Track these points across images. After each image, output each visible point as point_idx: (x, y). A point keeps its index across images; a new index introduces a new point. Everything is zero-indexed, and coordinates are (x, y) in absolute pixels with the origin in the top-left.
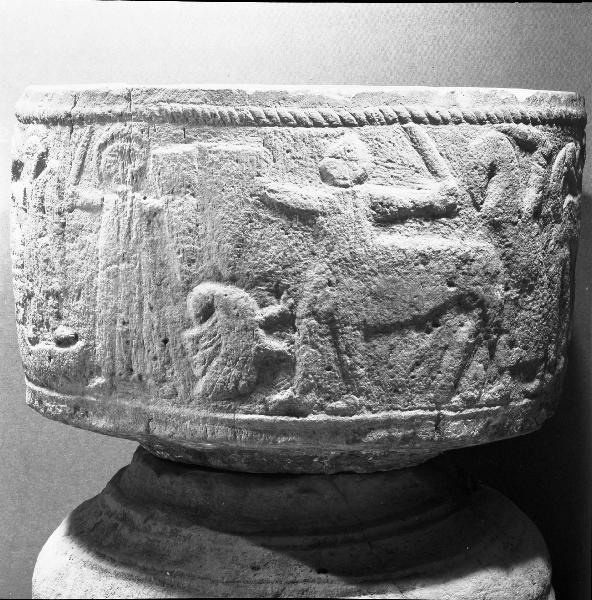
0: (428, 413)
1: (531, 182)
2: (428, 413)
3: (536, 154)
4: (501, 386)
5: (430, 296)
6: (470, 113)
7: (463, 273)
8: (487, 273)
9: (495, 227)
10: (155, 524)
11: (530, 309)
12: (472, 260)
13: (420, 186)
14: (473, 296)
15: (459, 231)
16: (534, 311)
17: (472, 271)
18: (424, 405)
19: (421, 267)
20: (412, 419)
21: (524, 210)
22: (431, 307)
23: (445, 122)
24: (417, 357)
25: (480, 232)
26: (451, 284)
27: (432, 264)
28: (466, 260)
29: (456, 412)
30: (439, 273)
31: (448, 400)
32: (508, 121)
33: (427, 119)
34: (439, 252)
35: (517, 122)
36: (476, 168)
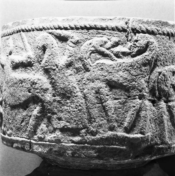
0: (26, 140)
1: (65, 53)
2: (26, 140)
3: (68, 42)
4: (55, 135)
5: (23, 96)
6: (37, 27)
7: (33, 88)
8: (42, 89)
9: (47, 71)
11: (69, 106)
13: (22, 55)
14: (37, 97)
15: (33, 72)
16: (72, 107)
17: (36, 87)
18: (25, 137)
19: (21, 85)
20: (22, 141)
21: (60, 65)
22: (24, 100)
23: (30, 31)
24: (22, 118)
25: (41, 72)
26: (30, 92)
27: (23, 84)
28: (34, 83)
29: (36, 141)
30: (25, 87)
31: (33, 137)
32: (52, 29)
33: (25, 30)
34: (25, 79)
35: (56, 29)
36: (37, 47)
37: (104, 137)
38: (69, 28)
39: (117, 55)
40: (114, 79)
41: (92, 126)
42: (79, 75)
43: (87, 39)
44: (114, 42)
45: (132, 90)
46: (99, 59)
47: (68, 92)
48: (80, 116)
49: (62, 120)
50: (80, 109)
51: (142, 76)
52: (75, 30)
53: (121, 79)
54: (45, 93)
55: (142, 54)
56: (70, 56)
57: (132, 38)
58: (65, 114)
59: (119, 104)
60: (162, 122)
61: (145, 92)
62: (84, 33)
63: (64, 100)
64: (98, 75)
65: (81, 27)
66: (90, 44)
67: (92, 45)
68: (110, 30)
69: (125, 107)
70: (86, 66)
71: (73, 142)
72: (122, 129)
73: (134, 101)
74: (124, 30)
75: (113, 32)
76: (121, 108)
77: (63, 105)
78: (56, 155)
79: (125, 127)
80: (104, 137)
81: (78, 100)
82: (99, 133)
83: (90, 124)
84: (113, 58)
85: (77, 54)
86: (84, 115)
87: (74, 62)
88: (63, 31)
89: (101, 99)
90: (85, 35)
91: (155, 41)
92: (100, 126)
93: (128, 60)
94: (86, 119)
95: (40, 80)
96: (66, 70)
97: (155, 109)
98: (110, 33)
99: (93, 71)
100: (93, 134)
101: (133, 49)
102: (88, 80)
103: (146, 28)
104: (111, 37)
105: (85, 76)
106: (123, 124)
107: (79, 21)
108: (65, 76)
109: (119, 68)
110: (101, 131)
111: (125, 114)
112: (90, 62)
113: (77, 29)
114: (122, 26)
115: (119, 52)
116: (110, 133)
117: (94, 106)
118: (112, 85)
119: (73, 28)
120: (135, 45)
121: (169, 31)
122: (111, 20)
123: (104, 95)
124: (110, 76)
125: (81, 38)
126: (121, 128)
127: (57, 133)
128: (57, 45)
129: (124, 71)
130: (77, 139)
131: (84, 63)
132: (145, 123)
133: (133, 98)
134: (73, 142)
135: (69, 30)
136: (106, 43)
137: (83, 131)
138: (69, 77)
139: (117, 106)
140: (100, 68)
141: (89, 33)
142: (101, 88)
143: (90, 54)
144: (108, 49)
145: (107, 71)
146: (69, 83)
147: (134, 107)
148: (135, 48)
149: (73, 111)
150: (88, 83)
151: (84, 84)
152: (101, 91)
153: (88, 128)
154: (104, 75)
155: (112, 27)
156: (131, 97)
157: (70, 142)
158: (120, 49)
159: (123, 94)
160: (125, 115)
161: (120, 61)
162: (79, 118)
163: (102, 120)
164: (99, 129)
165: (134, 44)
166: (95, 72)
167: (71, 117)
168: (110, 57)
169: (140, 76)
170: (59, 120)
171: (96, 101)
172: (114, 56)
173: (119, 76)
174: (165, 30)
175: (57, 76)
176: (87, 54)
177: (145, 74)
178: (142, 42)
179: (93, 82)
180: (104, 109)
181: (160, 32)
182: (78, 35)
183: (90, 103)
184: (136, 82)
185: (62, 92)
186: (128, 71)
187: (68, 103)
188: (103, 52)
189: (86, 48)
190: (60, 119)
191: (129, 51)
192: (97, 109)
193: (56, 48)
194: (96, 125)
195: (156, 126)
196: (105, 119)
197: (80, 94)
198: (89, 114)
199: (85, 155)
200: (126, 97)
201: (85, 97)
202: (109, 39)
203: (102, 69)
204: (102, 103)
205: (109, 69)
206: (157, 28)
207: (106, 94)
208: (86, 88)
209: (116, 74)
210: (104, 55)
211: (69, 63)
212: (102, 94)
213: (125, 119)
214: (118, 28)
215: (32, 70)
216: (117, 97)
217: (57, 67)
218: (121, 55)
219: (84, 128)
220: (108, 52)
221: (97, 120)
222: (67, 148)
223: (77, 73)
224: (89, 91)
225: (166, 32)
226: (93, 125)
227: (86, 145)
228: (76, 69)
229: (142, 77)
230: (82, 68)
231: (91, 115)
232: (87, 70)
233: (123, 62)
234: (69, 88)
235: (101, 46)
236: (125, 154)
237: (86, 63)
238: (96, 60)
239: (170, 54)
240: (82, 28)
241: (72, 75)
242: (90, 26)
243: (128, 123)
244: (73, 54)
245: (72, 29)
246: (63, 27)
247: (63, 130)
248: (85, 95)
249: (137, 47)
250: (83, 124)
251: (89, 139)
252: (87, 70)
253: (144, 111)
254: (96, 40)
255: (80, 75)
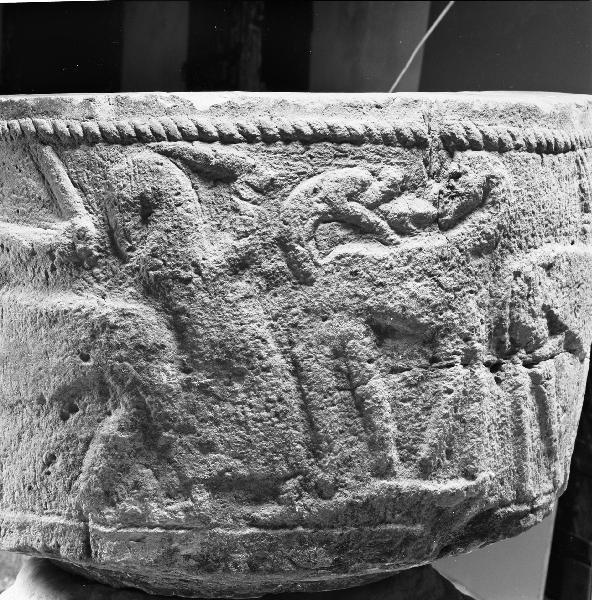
3: (237, 185)
8: (139, 347)
9: (154, 289)
10: (480, 305)
11: (243, 403)
12: (116, 327)
16: (251, 406)
25: (131, 289)
28: (106, 326)
32: (171, 138)
33: (238, 136)
37: (358, 497)
38: (238, 136)
39: (401, 227)
40: (392, 306)
41: (320, 466)
42: (275, 295)
43: (304, 173)
44: (390, 183)
45: (443, 337)
46: (342, 242)
47: (240, 355)
48: (282, 436)
49: (215, 452)
50: (282, 411)
51: (470, 289)
52: (262, 143)
53: (413, 303)
54: (150, 360)
55: (168, 91)
56: (246, 234)
57: (442, 166)
58: (227, 430)
59: (406, 386)
60: (519, 432)
61: (480, 341)
62: (293, 154)
63: (221, 382)
64: (341, 294)
65: (282, 132)
66: (315, 191)
67: (321, 194)
68: (376, 142)
69: (423, 395)
70: (300, 264)
71: (253, 522)
72: (412, 468)
73: (447, 372)
74: (419, 143)
75: (387, 149)
76: (410, 399)
77: (219, 399)
78: (189, 569)
79: (423, 460)
80: (358, 501)
81: (275, 380)
82: (342, 487)
83: (312, 460)
84: (388, 235)
85: (268, 225)
86: (294, 432)
87: (260, 253)
88: (217, 146)
89: (349, 376)
90: (296, 160)
91: (505, 173)
92: (347, 462)
93: (431, 242)
94: (299, 443)
95: (128, 314)
96: (231, 281)
97: (500, 391)
98: (378, 154)
99: (326, 283)
100: (322, 491)
101: (446, 203)
102: (307, 311)
103: (482, 132)
104: (379, 166)
105: (297, 299)
106: (414, 451)
107: (276, 113)
108: (227, 301)
109: (406, 268)
110: (348, 481)
111: (423, 417)
112: (315, 252)
113: (269, 140)
114: (414, 129)
115: (405, 215)
116: (378, 483)
117: (330, 398)
118: (384, 328)
119: (255, 136)
120: (452, 188)
121: (541, 135)
122: (378, 107)
123: (359, 361)
124: (380, 296)
125: (284, 172)
126: (410, 465)
127: (197, 495)
128: (192, 194)
129: (420, 276)
130: (268, 511)
131: (296, 258)
132: (479, 439)
133: (445, 363)
134: (253, 522)
135: (239, 144)
136: (364, 185)
137: (291, 484)
138: (242, 304)
139: (400, 394)
140: (346, 273)
141: (309, 152)
142: (352, 336)
143: (315, 225)
144: (372, 207)
145: (368, 280)
146: (242, 324)
147: (449, 392)
148: (452, 198)
149: (254, 419)
150: (309, 322)
151: (295, 325)
152: (350, 348)
153: (307, 472)
154: (360, 292)
155: (386, 131)
156: (441, 361)
157: (242, 522)
158: (404, 205)
159: (416, 352)
160: (420, 420)
161: (408, 244)
162: (278, 440)
163: (352, 444)
164: (342, 474)
165: (448, 187)
166: (331, 287)
167: (249, 440)
168: (377, 234)
169: (465, 290)
170: (205, 452)
171: (333, 382)
172: (389, 231)
173: (408, 295)
174: (531, 133)
175: (199, 306)
176: (306, 226)
177: (479, 282)
178: (474, 179)
179: (324, 319)
180: (361, 407)
181: (519, 141)
182: (271, 162)
183: (316, 390)
184: (453, 310)
185: (215, 357)
186: (433, 276)
187: (236, 392)
188: (358, 217)
189: (302, 207)
190: (207, 447)
191: (433, 210)
192: (336, 408)
193: (191, 206)
194: (332, 461)
195: (503, 445)
196: (360, 439)
197: (278, 360)
198: (311, 425)
199: (293, 563)
200: (424, 362)
201: (297, 370)
202: (373, 174)
203: (355, 273)
204: (352, 390)
205: (375, 273)
206: (512, 129)
207: (366, 357)
208: (302, 340)
209: (395, 288)
210: (361, 229)
211: (243, 259)
212: (353, 358)
213: (423, 433)
214: (402, 134)
215: (92, 281)
216: (400, 364)
217: (198, 272)
218: (410, 225)
219: (294, 476)
220: (372, 217)
221: (338, 444)
222: (232, 545)
223: (268, 290)
224: (311, 350)
225: (533, 141)
226: (325, 462)
227: (300, 529)
228: (266, 276)
229: (471, 292)
230: (285, 274)
231: (319, 429)
232: (306, 280)
233: (420, 246)
234: (243, 341)
235: (351, 197)
236: (419, 546)
237: (302, 256)
238: (334, 243)
239: (543, 210)
240: (286, 138)
241: (251, 297)
242: (314, 130)
243: (431, 445)
244: (256, 225)
245: (249, 139)
246: (216, 134)
247: (218, 485)
248: (295, 363)
249: (459, 194)
250: (292, 461)
251: (309, 510)
252: (306, 280)
253: (474, 402)
254: (334, 177)
255: (280, 298)
